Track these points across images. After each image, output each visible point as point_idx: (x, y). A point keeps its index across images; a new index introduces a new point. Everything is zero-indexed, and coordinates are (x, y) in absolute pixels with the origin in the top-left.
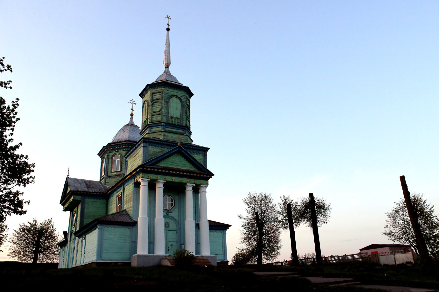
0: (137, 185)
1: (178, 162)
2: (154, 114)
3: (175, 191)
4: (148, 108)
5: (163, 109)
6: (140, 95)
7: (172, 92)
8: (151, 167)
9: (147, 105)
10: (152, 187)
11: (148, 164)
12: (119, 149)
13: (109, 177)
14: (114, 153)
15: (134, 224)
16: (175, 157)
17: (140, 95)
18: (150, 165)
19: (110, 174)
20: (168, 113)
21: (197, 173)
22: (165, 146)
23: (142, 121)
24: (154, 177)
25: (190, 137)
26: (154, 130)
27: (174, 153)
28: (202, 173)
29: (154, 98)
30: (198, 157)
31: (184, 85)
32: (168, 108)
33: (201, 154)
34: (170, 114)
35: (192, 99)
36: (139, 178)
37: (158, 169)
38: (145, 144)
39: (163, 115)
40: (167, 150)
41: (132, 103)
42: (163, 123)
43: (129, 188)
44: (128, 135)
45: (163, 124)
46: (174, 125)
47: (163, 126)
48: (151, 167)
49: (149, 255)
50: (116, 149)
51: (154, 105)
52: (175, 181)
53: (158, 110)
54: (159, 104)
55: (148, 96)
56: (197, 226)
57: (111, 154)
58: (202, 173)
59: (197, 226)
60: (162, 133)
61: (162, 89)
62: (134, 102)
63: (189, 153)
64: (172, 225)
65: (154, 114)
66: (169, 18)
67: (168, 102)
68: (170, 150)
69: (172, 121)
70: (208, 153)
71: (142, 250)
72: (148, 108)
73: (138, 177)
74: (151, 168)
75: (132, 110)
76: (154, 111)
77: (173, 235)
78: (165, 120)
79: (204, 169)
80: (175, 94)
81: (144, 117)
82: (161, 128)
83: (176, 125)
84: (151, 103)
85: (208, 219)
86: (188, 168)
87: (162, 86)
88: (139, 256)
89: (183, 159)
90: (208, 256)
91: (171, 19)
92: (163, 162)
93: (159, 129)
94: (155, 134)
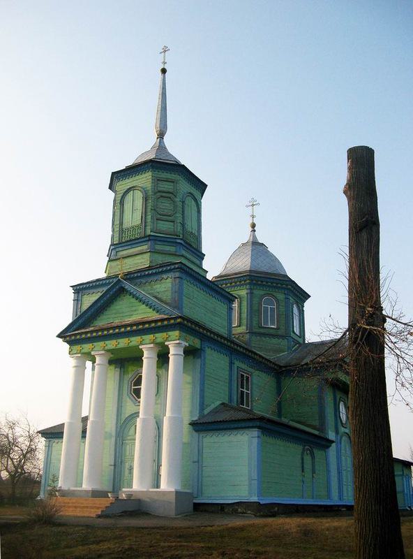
10: (163, 358)
16: (121, 303)
24: (160, 337)
37: (102, 330)
68: (100, 294)
74: (75, 335)
75: (253, 217)
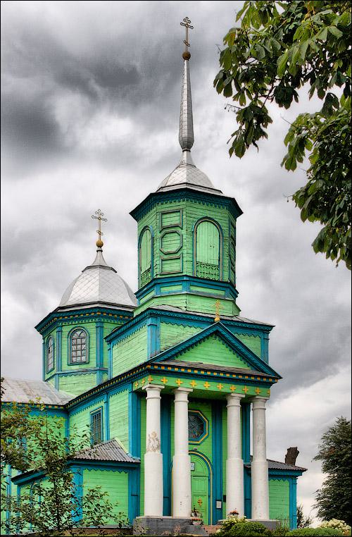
0: (141, 395)
1: (214, 355)
2: (166, 257)
3: (209, 409)
4: (153, 244)
5: (184, 248)
6: (132, 213)
7: (201, 210)
8: (166, 363)
9: (149, 237)
11: (162, 359)
12: (83, 318)
13: (66, 374)
14: (71, 327)
15: (133, 469)
17: (132, 213)
18: (165, 360)
19: (66, 368)
20: (194, 255)
21: (250, 376)
22: (190, 324)
23: (140, 269)
25: (234, 302)
26: (165, 290)
27: (207, 337)
28: (261, 374)
29: (165, 224)
30: (251, 343)
31: (226, 193)
32: (194, 244)
33: (258, 338)
34: (199, 259)
35: (240, 221)
36: (143, 384)
37: (180, 367)
38: (154, 319)
39: (185, 259)
40: (191, 332)
41: (100, 219)
42: (186, 276)
43: (120, 403)
44: (185, 176)
45: (185, 278)
46: (206, 279)
47: (185, 283)
48: (166, 363)
49: (271, 520)
50: (76, 319)
51: (165, 239)
52: (209, 389)
53: (174, 249)
54: (175, 236)
55: (151, 219)
56: (248, 471)
57: (66, 329)
58: (261, 374)
59: (248, 471)
60: (184, 297)
61: (182, 204)
62: (102, 214)
63: (236, 335)
64: (202, 468)
65: (166, 257)
66: (187, 26)
67: (194, 233)
69: (203, 273)
70: (272, 335)
71: (152, 507)
72: (153, 244)
73: (142, 381)
74: (167, 366)
75: (100, 233)
76: (165, 251)
77: (203, 486)
78: (190, 270)
79: (263, 367)
80: (208, 214)
81: (143, 261)
82: (181, 287)
83: (210, 280)
84: (159, 235)
85: (267, 458)
86: (188, 336)
87: (181, 197)
88: (149, 520)
89: (203, 344)
90: (266, 522)
91: (192, 27)
92: (188, 354)
93: (177, 288)
94: (169, 299)
